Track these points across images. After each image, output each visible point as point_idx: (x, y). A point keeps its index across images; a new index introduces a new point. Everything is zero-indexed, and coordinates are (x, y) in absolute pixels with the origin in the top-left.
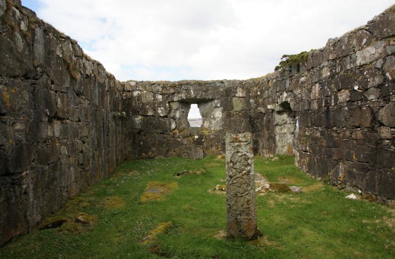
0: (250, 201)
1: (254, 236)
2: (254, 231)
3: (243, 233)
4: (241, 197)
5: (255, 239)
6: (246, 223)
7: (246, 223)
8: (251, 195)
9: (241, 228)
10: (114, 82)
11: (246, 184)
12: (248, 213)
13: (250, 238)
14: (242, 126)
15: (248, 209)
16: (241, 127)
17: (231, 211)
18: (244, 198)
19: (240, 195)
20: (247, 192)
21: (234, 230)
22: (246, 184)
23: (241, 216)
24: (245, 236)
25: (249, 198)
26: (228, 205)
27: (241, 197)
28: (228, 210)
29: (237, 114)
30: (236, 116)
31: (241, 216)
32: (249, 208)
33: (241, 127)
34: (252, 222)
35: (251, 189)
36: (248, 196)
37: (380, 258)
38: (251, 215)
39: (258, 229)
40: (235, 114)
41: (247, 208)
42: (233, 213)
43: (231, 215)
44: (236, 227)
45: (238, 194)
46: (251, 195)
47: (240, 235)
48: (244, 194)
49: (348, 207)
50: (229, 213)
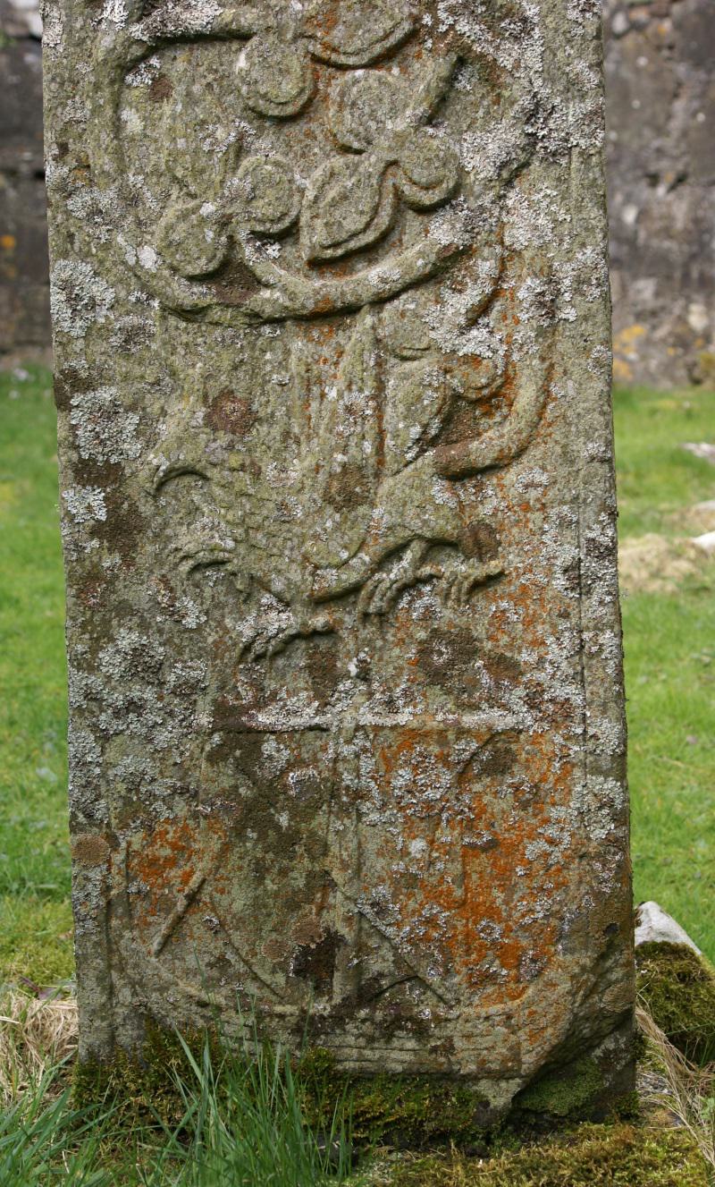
0: (492, 400)
1: (559, 1065)
2: (566, 965)
3: (367, 994)
4: (335, 315)
5: (594, 1111)
6: (431, 816)
7: (431, 816)
8: (527, 288)
9: (336, 918)
10: (615, 593)
11: (429, 68)
12: (465, 647)
13: (500, 1096)
14: (676, 125)
15: (458, 567)
16: (660, 131)
17: (142, 593)
18: (386, 351)
19: (311, 289)
20: (443, 232)
21: (199, 947)
22: (429, 68)
23: (324, 678)
24: (401, 1053)
25: (474, 343)
26: (87, 473)
27: (335, 315)
28: (87, 581)
29: (635, 27)
30: (630, 41)
31: (324, 678)
32: (479, 542)
33: (660, 131)
34: (532, 800)
35: (510, 174)
36: (459, 303)
37: (711, 763)
38: (504, 667)
39: (655, 923)
40: (619, 24)
41: (437, 545)
42: (184, 640)
43: (142, 667)
44: (238, 899)
45: (265, 261)
46: (527, 288)
47: (307, 1027)
48: (373, 276)
49: (311, 875)
50: (101, 636)
